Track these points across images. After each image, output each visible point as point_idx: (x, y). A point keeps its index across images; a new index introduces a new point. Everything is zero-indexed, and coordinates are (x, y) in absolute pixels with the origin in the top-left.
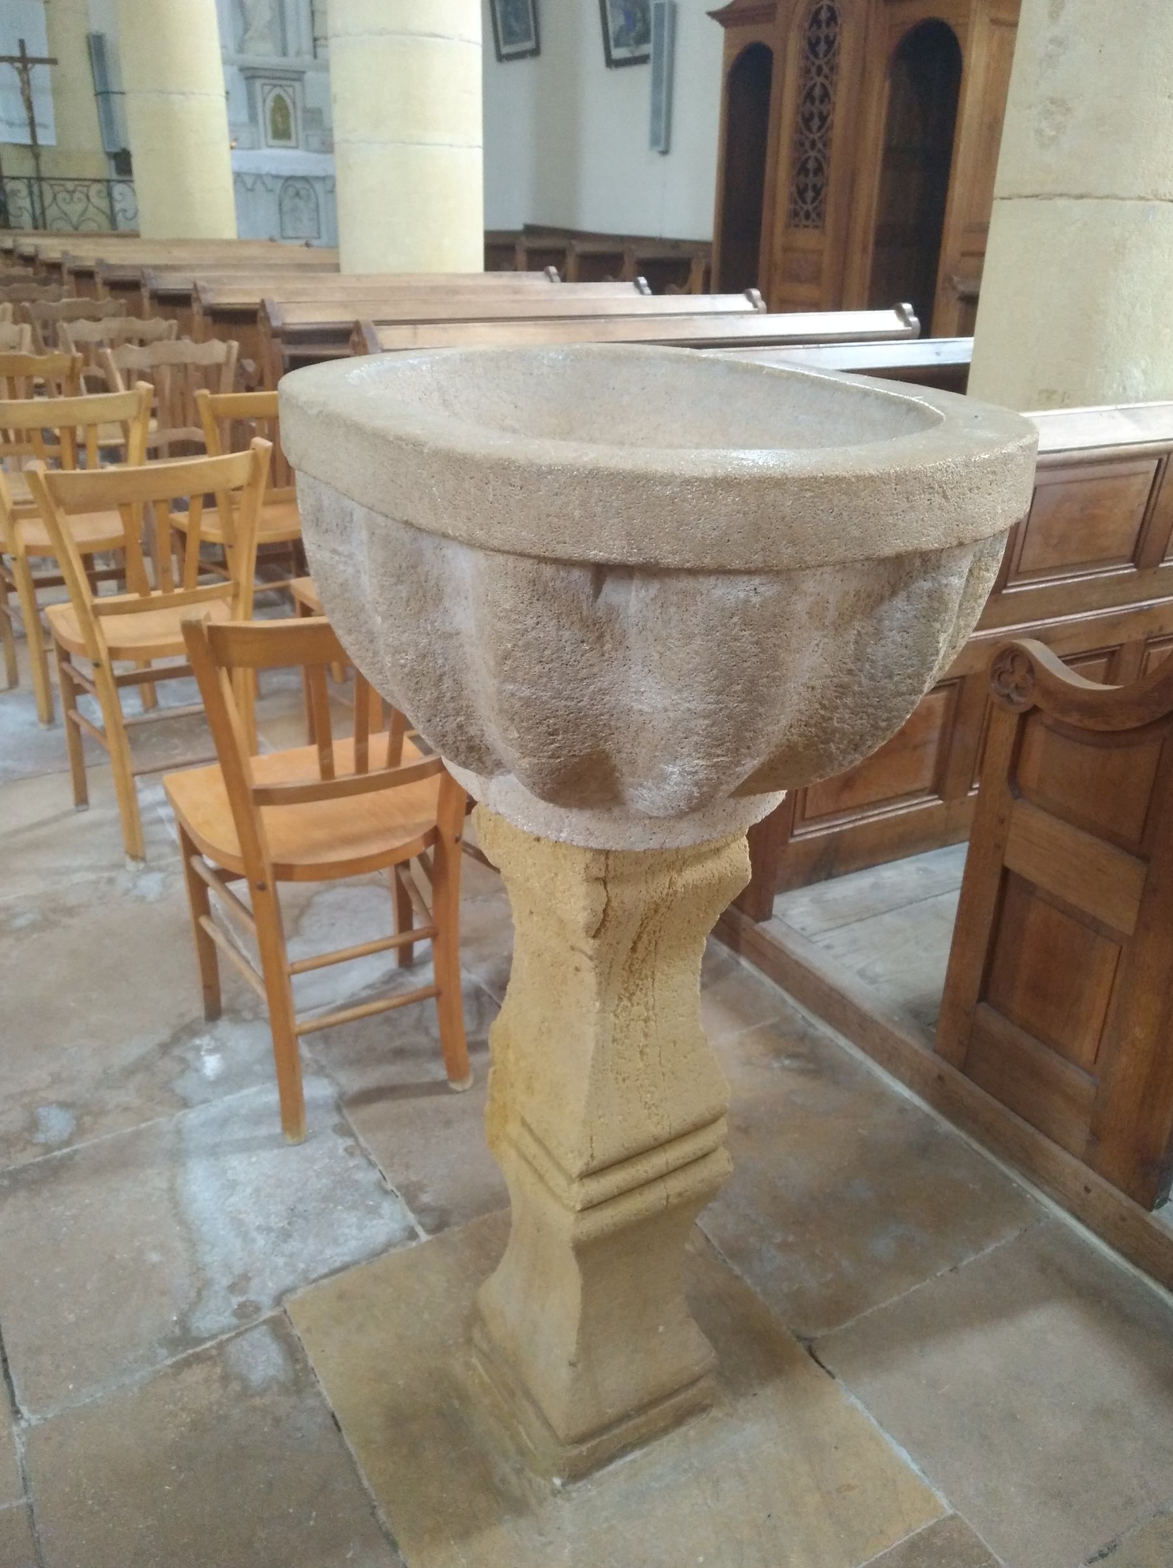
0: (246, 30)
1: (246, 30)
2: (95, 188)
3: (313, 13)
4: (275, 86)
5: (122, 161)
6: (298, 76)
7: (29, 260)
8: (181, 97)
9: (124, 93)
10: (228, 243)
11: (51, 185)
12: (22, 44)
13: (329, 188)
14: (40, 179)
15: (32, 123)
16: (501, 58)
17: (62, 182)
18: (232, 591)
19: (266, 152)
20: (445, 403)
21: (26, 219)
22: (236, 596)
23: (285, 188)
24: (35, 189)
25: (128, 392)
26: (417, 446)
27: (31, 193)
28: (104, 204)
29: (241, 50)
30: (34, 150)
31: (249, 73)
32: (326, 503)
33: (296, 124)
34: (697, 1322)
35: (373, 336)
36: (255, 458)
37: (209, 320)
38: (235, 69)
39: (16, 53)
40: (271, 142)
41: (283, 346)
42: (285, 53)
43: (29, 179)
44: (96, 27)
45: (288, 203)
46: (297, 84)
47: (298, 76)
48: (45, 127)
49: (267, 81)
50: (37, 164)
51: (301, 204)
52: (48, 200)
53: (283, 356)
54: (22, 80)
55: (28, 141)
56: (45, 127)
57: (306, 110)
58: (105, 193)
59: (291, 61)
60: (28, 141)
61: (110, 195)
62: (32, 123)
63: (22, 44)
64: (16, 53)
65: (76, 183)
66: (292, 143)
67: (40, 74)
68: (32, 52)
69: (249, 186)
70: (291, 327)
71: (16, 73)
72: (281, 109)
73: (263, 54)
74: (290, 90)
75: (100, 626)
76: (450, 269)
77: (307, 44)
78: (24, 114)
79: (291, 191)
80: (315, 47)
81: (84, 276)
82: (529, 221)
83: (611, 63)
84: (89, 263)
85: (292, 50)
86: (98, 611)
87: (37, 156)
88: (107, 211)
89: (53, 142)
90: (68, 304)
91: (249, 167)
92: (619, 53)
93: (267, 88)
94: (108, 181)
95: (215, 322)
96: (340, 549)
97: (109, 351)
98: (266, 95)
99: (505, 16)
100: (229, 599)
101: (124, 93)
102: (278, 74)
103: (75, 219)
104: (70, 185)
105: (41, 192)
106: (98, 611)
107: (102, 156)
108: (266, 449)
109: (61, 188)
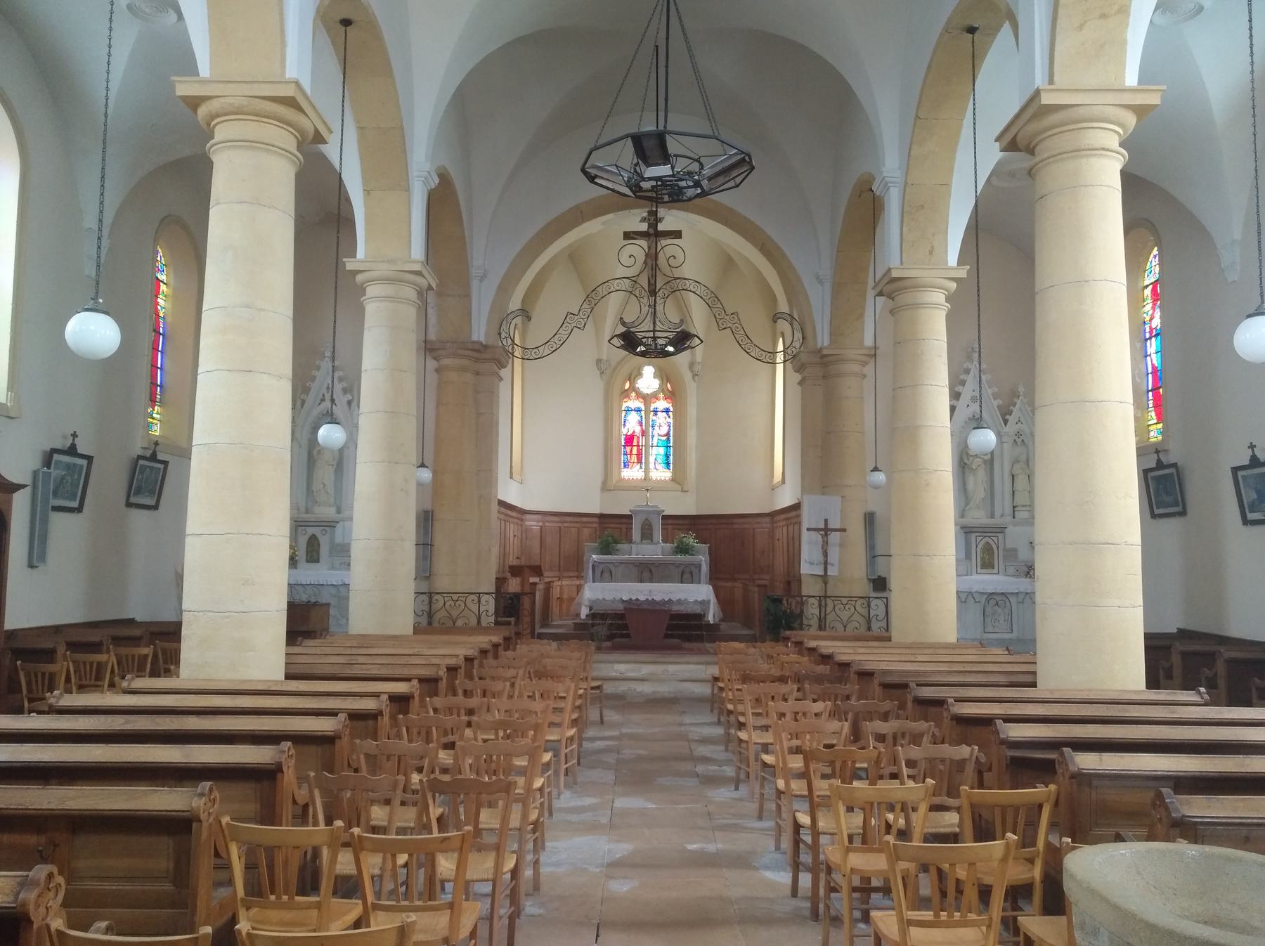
0: (967, 504)
1: (967, 504)
2: (861, 601)
3: (1013, 492)
4: (985, 537)
5: (880, 584)
6: (1002, 530)
7: (826, 659)
8: (927, 558)
9: (890, 556)
10: (948, 646)
11: (833, 600)
12: (826, 521)
13: (1021, 600)
14: (826, 597)
15: (826, 563)
16: (1154, 516)
17: (839, 599)
18: (987, 922)
19: (975, 577)
20: (1139, 873)
21: (814, 622)
22: (989, 926)
23: (988, 600)
24: (823, 603)
25: (125, 7)
26: (1134, 916)
27: (820, 605)
28: (864, 611)
29: (962, 516)
30: (824, 578)
31: (967, 530)
32: (1087, 921)
33: (999, 561)
34: (1152, 927)
35: (1072, 758)
36: (1007, 845)
37: (954, 722)
38: (958, 527)
39: (822, 526)
40: (979, 570)
41: (1006, 750)
42: (992, 516)
43: (820, 597)
44: (871, 508)
45: (989, 610)
46: (1000, 536)
47: (1002, 530)
48: (833, 565)
49: (978, 534)
50: (826, 588)
51: (1000, 610)
52: (829, 609)
53: (1006, 756)
54: (823, 541)
55: (822, 573)
56: (833, 565)
57: (1005, 550)
58: (866, 605)
59: (997, 521)
60: (822, 573)
61: (869, 606)
62: (826, 563)
63: (826, 521)
64: (822, 526)
65: (849, 599)
66: (995, 571)
67: (834, 538)
68: (831, 526)
69: (963, 600)
70: (1012, 739)
71: (820, 536)
72: (988, 549)
73: (978, 517)
74: (995, 539)
75: (909, 932)
76: (1119, 686)
77: (1008, 510)
78: (821, 559)
79: (993, 602)
80: (1014, 511)
81: (866, 675)
82: (1182, 627)
83: (1246, 522)
84: (869, 667)
85: (997, 514)
86: (910, 923)
87: (826, 583)
88: (867, 615)
89: (836, 574)
90: (864, 704)
91: (965, 588)
92: (1251, 516)
93: (979, 539)
94: (869, 598)
95: (957, 723)
96: (1093, 942)
97: (900, 748)
98: (978, 543)
99: (1157, 491)
100: (984, 928)
101: (890, 556)
102: (987, 530)
103: (845, 621)
104: (845, 601)
105: (826, 605)
106: (910, 923)
107: (866, 581)
108: (1014, 841)
109: (839, 602)
